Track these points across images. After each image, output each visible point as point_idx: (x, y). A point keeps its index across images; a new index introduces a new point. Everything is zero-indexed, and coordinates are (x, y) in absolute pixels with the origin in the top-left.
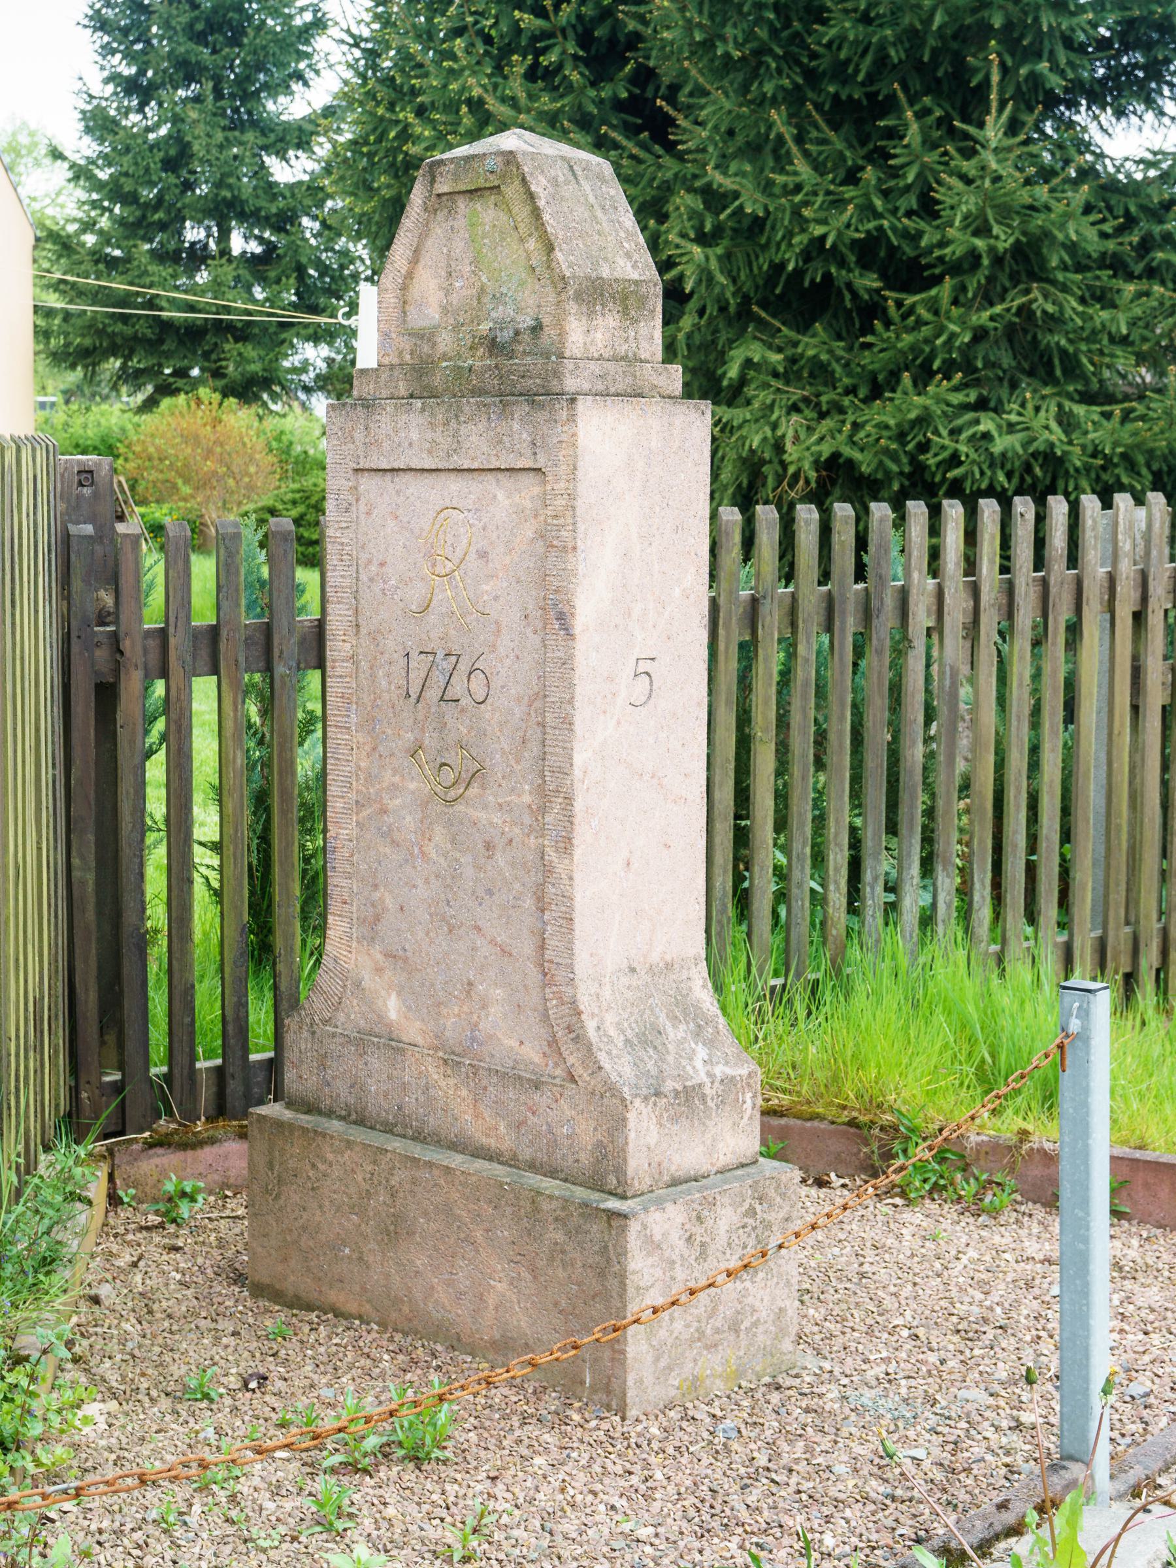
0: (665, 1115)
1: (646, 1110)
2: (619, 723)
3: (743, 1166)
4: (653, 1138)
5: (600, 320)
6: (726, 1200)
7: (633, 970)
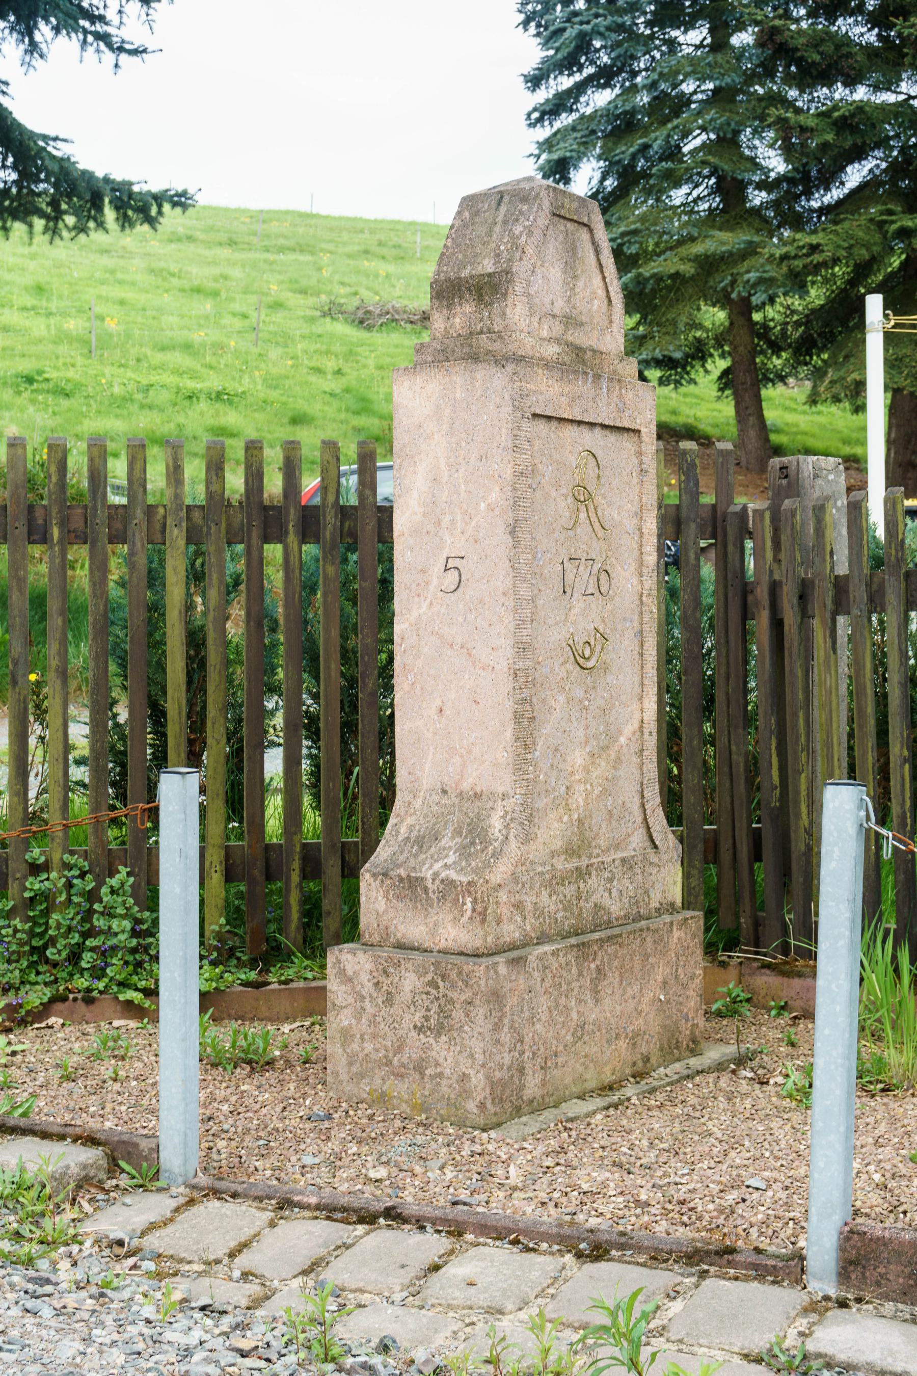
0: (391, 893)
1: (375, 884)
2: (431, 604)
3: (461, 954)
4: (381, 905)
5: (458, 309)
6: (410, 966)
7: (445, 792)
